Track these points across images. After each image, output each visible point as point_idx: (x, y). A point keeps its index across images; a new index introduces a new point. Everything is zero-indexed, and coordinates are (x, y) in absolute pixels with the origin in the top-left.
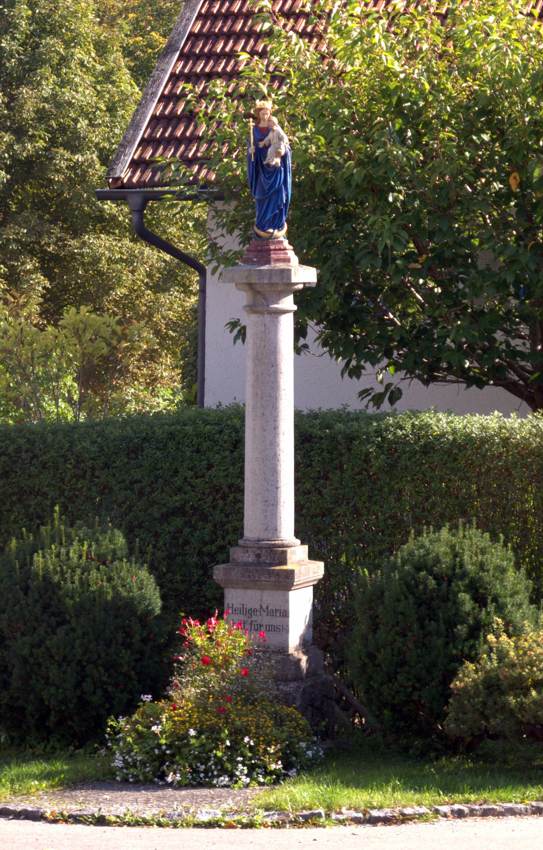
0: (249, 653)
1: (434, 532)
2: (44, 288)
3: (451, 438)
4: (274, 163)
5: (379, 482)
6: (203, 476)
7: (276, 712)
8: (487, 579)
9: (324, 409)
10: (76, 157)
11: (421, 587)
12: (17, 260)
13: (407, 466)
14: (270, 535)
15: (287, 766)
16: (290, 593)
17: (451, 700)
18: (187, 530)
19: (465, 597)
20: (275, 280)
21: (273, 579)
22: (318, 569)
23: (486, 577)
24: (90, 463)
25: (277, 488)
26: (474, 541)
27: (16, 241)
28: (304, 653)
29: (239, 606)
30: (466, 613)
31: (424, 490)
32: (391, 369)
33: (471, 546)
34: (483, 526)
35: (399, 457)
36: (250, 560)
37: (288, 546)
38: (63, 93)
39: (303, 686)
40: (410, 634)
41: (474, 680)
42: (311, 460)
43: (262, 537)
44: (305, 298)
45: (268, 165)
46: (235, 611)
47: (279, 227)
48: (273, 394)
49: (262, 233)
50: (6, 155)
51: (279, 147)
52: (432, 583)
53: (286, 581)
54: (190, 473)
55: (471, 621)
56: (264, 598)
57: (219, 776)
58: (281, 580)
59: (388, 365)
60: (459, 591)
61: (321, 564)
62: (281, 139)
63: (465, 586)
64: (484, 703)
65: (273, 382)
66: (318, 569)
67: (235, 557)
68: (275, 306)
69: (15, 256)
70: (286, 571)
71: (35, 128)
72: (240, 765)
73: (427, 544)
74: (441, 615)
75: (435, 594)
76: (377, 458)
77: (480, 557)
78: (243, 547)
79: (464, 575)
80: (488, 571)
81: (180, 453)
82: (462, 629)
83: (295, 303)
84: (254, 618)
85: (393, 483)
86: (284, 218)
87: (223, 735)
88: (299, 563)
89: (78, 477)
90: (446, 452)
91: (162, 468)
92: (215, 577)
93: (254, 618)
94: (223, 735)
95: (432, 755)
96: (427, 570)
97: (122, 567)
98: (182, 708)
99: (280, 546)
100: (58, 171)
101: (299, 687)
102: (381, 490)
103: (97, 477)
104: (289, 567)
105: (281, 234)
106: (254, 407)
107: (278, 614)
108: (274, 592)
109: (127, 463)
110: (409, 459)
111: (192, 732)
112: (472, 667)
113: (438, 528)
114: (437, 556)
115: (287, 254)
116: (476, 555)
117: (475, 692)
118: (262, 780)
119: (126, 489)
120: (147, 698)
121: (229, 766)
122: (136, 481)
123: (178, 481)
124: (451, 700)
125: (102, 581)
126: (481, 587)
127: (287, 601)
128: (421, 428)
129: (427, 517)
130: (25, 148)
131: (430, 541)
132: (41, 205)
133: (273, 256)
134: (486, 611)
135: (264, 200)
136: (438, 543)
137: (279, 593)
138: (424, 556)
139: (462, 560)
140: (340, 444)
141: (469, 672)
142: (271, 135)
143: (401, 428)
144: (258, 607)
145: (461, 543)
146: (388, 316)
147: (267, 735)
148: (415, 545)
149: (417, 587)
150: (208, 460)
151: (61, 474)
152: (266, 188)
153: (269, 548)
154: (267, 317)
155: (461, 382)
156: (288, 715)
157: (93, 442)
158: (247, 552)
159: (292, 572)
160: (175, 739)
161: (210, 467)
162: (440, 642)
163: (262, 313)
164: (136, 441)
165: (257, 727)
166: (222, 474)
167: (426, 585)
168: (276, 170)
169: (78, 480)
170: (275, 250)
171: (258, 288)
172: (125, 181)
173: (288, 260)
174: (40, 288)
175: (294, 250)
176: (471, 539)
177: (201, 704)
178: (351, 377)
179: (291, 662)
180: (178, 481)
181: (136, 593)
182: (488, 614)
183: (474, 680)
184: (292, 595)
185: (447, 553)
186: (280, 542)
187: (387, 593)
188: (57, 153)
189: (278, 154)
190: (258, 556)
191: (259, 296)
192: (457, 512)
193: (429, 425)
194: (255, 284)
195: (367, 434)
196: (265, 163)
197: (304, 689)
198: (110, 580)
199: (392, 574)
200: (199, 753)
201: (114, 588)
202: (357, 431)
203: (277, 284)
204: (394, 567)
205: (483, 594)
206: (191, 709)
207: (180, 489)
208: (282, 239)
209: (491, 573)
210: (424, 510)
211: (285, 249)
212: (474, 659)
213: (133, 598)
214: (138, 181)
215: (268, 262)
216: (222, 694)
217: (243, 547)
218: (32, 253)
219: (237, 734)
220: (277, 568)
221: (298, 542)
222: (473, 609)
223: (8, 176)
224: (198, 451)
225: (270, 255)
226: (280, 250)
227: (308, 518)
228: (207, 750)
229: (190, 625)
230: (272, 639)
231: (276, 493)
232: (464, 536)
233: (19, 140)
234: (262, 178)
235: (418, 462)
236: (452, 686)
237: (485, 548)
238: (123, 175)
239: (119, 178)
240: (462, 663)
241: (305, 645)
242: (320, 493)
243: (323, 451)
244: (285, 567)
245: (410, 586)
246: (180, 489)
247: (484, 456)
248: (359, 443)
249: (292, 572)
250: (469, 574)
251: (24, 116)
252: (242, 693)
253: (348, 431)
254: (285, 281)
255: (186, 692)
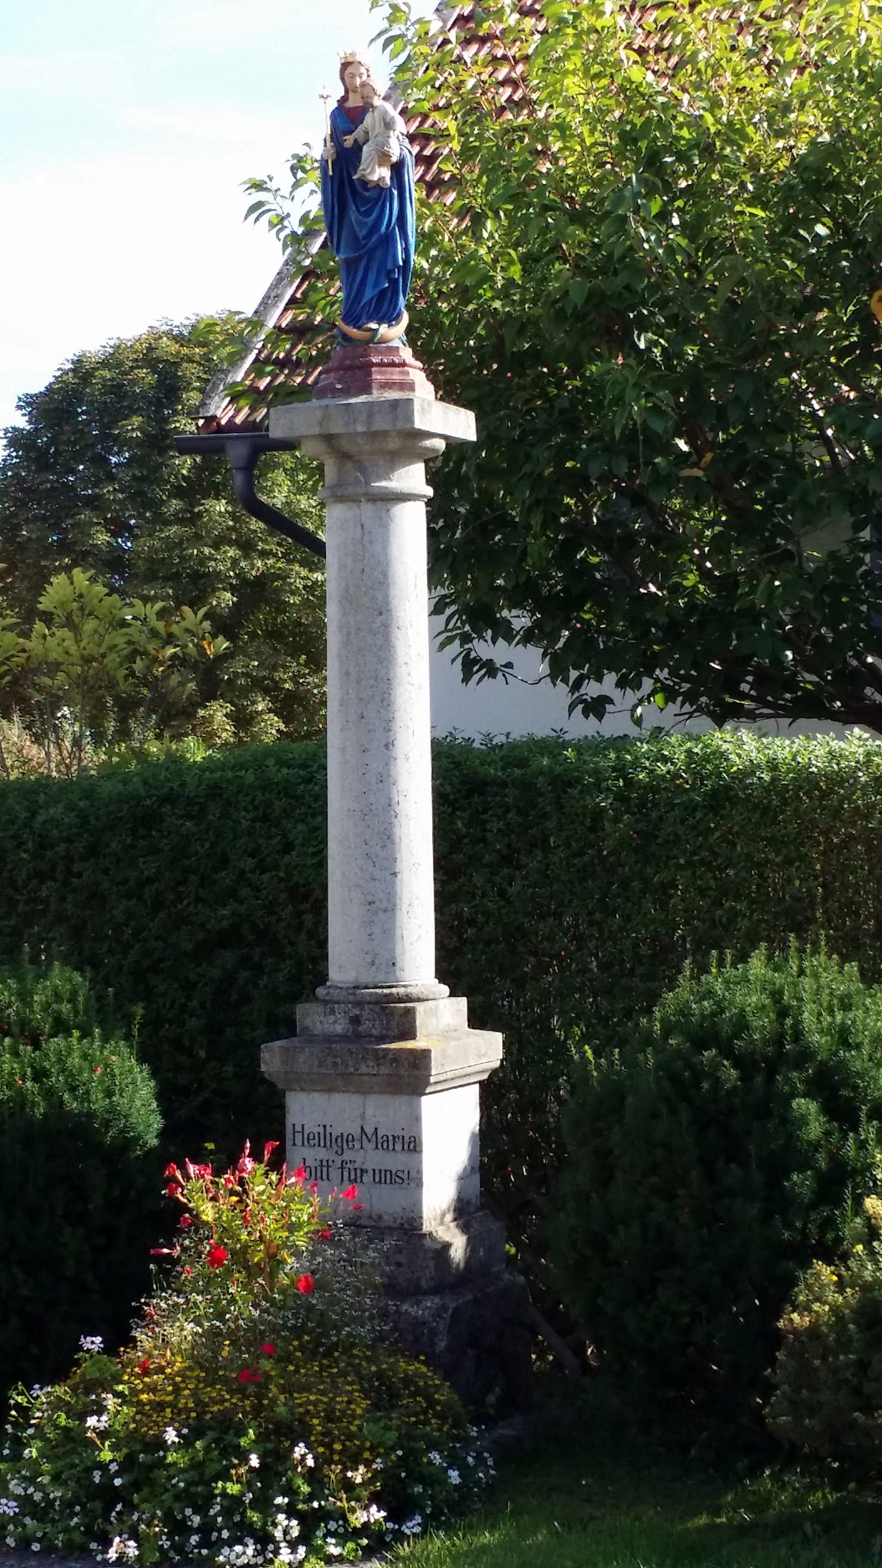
0: (323, 1237)
1: (734, 965)
2: (278, 731)
3: (766, 777)
4: (375, 177)
5: (620, 870)
6: (277, 867)
7: (380, 1376)
8: (857, 1066)
9: (515, 736)
10: (315, 576)
11: (705, 1085)
12: (246, 698)
13: (677, 836)
14: (380, 977)
15: (396, 1515)
16: (424, 1099)
17: (780, 1355)
18: (244, 974)
19: (805, 1106)
20: (380, 424)
21: (385, 1070)
22: (489, 1049)
23: (857, 1061)
24: (61, 848)
25: (395, 874)
26: (823, 981)
27: (246, 675)
28: (465, 1228)
29: (316, 1130)
30: (810, 1143)
31: (712, 883)
32: (659, 698)
33: (818, 992)
34: (846, 948)
35: (661, 819)
36: (339, 1029)
37: (419, 1000)
38: (299, 501)
39: (452, 1305)
40: (681, 1192)
41: (835, 1310)
42: (485, 830)
43: (364, 979)
44: (449, 470)
45: (364, 183)
46: (308, 1140)
47: (391, 318)
48: (382, 673)
49: (353, 332)
50: (232, 573)
51: (386, 143)
52: (731, 1074)
53: (412, 1076)
54: (249, 863)
55: (822, 1161)
56: (370, 1112)
57: (231, 1543)
58: (403, 1072)
59: (653, 693)
60: (793, 1096)
61: (498, 1038)
62: (388, 125)
63: (807, 1082)
64: (863, 1366)
65: (381, 648)
66: (489, 1049)
67: (308, 1022)
68: (384, 484)
69: (245, 692)
70: (412, 1051)
71: (265, 541)
72: (281, 1517)
73: (719, 988)
74: (752, 1148)
75: (737, 1101)
76: (616, 820)
77: (839, 1017)
78: (325, 1002)
79: (805, 1055)
80: (858, 1047)
81: (231, 823)
82: (801, 1182)
83: (429, 482)
84: (348, 1155)
85: (649, 870)
86: (402, 302)
87: (243, 1442)
88: (446, 1035)
89: (41, 876)
90: (756, 806)
91: (197, 853)
92: (263, 1068)
93: (348, 1155)
94: (243, 1442)
95: (742, 1465)
96: (718, 1047)
97: (70, 1049)
98: (161, 1370)
99: (400, 1000)
100: (293, 593)
101: (444, 1308)
102: (625, 885)
103: (79, 875)
104: (418, 1044)
105: (395, 333)
106: (342, 703)
107: (398, 1147)
108: (389, 1099)
109: (131, 846)
110: (683, 822)
111: (171, 1436)
112: (826, 1272)
113: (742, 957)
114: (742, 1014)
115: (408, 373)
116: (831, 1012)
117: (837, 1340)
118: (334, 1550)
119: (128, 896)
120: (93, 1343)
121: (255, 1517)
122: (150, 881)
123: (225, 878)
124: (780, 1355)
125: (23, 1078)
126: (844, 1083)
127: (416, 1119)
128: (706, 759)
129: (722, 936)
130: (253, 566)
131: (727, 982)
132: (274, 634)
133: (377, 376)
134: (856, 1140)
135: (358, 260)
136: (745, 985)
137: (398, 1103)
138: (713, 1014)
139: (797, 1023)
140: (541, 794)
141: (822, 1287)
142: (368, 119)
143: (665, 760)
144: (357, 1133)
145: (795, 985)
146: (647, 588)
147: (351, 1437)
148: (692, 992)
149: (697, 1085)
150: (285, 836)
151: (10, 871)
152: (362, 234)
153: (377, 1003)
154: (367, 509)
155: (781, 716)
156: (408, 1381)
157: (70, 808)
158: (332, 1012)
159: (424, 1056)
160: (138, 1447)
161: (288, 847)
162: (754, 1210)
163: (354, 500)
164: (148, 802)
165: (330, 1417)
166: (309, 862)
167: (717, 1083)
168: (380, 193)
169: (42, 882)
170: (381, 365)
171: (346, 445)
172: (223, 422)
173: (410, 386)
174: (274, 732)
175: (423, 369)
176: (816, 976)
177: (204, 1362)
178: (587, 717)
179: (426, 1251)
180: (225, 878)
181: (99, 1102)
182: (862, 1145)
183: (835, 1310)
184: (428, 1104)
185: (764, 1006)
186: (401, 990)
187: (630, 1100)
188: (292, 570)
189: (383, 157)
190: (355, 1021)
191: (349, 465)
192: (784, 924)
193: (722, 754)
194: (338, 435)
195: (597, 773)
196: (355, 177)
197: (456, 1310)
198: (40, 1075)
199: (641, 1057)
200: (189, 1484)
201: (49, 1094)
202: (577, 769)
203: (385, 434)
204: (648, 1040)
205: (848, 1099)
206: (181, 1373)
207: (233, 893)
208: (396, 343)
209: (866, 1051)
210: (714, 924)
211: (403, 364)
212: (834, 1254)
213: (91, 1115)
214: (245, 421)
215: (366, 389)
216: (253, 1338)
217: (325, 1002)
218: (266, 691)
219: (279, 1436)
220: (393, 1046)
221: (445, 989)
222: (827, 1133)
223: (235, 599)
224: (265, 818)
225: (370, 374)
226: (393, 364)
227: (480, 946)
228: (207, 1476)
229: (187, 1177)
230: (384, 1202)
231: (393, 884)
232: (801, 972)
233: (246, 556)
234: (353, 215)
235: (701, 828)
236: (781, 1324)
237: (849, 996)
238: (219, 413)
239: (214, 418)
240: (806, 1265)
241: (463, 1211)
242: (502, 894)
243: (508, 812)
244: (409, 1045)
245: (681, 1082)
246: (233, 893)
247: (837, 812)
248: (581, 792)
249: (424, 1056)
250: (814, 1054)
251: (252, 527)
252: (298, 1331)
253: (558, 769)
254: (400, 425)
255: (171, 1333)
